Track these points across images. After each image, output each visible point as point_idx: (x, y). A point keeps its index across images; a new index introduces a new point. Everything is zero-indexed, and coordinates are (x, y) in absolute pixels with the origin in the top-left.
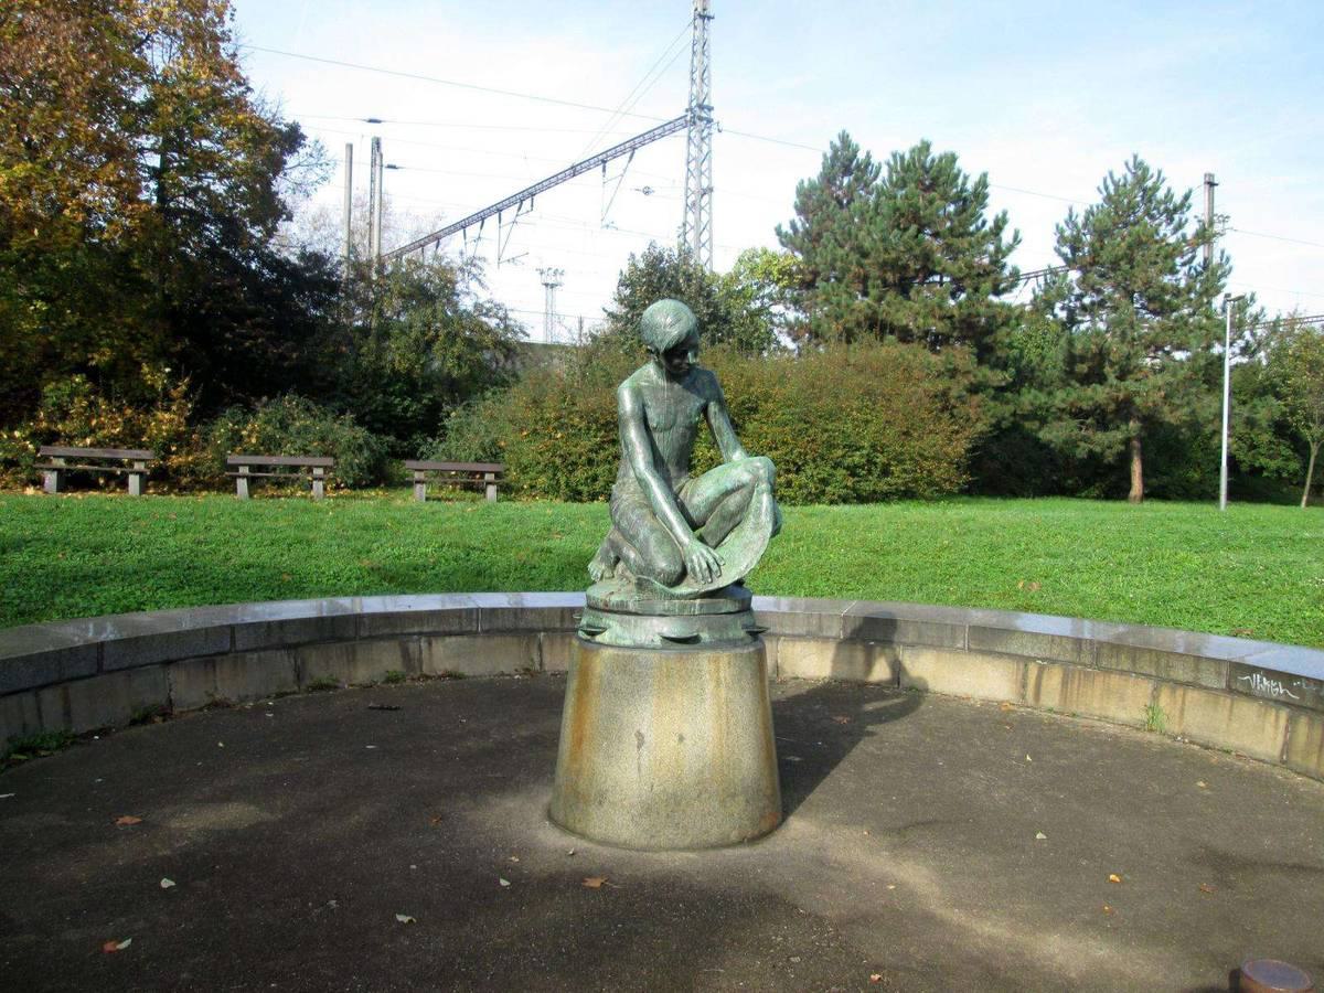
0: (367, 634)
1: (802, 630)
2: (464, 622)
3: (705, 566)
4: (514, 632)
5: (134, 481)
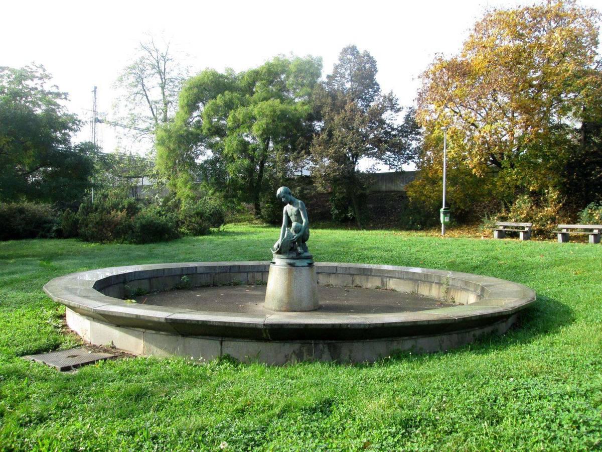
4: (411, 279)
5: (521, 235)
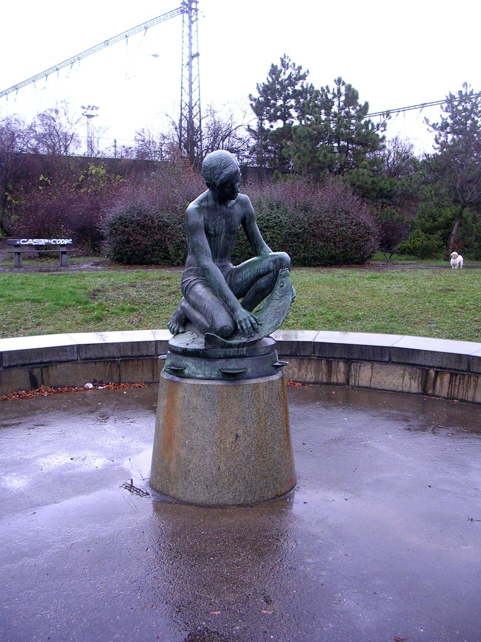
0: (7, 365)
1: (288, 352)
2: (69, 354)
3: (249, 325)
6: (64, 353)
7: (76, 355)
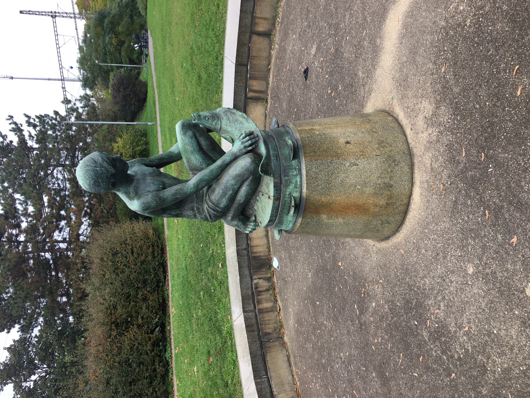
3: (247, 138)
6: (263, 390)
7: (263, 380)
